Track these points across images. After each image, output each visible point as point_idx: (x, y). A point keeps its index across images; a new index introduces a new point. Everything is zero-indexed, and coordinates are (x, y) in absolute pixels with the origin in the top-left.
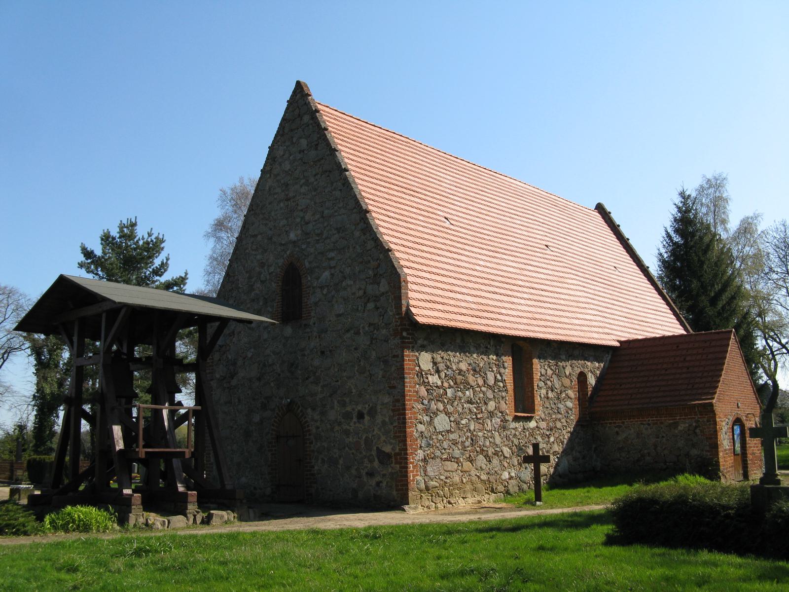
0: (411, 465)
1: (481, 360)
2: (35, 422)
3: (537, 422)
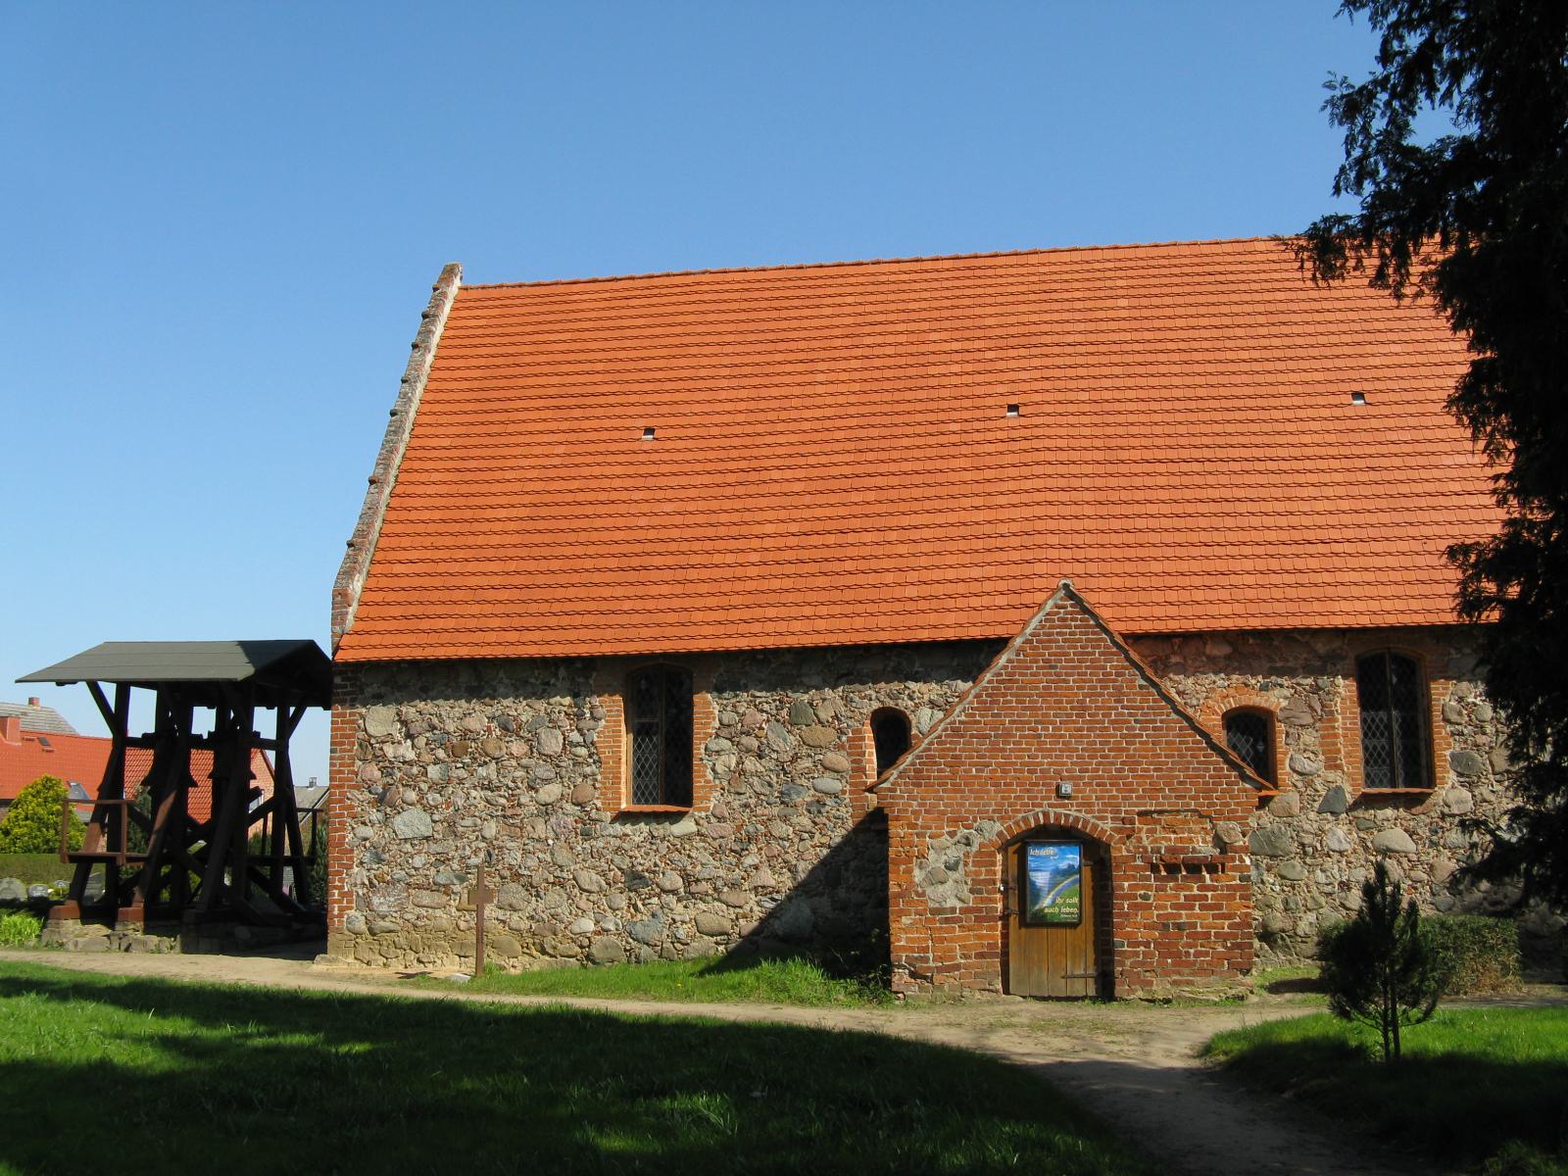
0: (336, 892)
1: (522, 710)
2: (1484, 100)
3: (697, 824)
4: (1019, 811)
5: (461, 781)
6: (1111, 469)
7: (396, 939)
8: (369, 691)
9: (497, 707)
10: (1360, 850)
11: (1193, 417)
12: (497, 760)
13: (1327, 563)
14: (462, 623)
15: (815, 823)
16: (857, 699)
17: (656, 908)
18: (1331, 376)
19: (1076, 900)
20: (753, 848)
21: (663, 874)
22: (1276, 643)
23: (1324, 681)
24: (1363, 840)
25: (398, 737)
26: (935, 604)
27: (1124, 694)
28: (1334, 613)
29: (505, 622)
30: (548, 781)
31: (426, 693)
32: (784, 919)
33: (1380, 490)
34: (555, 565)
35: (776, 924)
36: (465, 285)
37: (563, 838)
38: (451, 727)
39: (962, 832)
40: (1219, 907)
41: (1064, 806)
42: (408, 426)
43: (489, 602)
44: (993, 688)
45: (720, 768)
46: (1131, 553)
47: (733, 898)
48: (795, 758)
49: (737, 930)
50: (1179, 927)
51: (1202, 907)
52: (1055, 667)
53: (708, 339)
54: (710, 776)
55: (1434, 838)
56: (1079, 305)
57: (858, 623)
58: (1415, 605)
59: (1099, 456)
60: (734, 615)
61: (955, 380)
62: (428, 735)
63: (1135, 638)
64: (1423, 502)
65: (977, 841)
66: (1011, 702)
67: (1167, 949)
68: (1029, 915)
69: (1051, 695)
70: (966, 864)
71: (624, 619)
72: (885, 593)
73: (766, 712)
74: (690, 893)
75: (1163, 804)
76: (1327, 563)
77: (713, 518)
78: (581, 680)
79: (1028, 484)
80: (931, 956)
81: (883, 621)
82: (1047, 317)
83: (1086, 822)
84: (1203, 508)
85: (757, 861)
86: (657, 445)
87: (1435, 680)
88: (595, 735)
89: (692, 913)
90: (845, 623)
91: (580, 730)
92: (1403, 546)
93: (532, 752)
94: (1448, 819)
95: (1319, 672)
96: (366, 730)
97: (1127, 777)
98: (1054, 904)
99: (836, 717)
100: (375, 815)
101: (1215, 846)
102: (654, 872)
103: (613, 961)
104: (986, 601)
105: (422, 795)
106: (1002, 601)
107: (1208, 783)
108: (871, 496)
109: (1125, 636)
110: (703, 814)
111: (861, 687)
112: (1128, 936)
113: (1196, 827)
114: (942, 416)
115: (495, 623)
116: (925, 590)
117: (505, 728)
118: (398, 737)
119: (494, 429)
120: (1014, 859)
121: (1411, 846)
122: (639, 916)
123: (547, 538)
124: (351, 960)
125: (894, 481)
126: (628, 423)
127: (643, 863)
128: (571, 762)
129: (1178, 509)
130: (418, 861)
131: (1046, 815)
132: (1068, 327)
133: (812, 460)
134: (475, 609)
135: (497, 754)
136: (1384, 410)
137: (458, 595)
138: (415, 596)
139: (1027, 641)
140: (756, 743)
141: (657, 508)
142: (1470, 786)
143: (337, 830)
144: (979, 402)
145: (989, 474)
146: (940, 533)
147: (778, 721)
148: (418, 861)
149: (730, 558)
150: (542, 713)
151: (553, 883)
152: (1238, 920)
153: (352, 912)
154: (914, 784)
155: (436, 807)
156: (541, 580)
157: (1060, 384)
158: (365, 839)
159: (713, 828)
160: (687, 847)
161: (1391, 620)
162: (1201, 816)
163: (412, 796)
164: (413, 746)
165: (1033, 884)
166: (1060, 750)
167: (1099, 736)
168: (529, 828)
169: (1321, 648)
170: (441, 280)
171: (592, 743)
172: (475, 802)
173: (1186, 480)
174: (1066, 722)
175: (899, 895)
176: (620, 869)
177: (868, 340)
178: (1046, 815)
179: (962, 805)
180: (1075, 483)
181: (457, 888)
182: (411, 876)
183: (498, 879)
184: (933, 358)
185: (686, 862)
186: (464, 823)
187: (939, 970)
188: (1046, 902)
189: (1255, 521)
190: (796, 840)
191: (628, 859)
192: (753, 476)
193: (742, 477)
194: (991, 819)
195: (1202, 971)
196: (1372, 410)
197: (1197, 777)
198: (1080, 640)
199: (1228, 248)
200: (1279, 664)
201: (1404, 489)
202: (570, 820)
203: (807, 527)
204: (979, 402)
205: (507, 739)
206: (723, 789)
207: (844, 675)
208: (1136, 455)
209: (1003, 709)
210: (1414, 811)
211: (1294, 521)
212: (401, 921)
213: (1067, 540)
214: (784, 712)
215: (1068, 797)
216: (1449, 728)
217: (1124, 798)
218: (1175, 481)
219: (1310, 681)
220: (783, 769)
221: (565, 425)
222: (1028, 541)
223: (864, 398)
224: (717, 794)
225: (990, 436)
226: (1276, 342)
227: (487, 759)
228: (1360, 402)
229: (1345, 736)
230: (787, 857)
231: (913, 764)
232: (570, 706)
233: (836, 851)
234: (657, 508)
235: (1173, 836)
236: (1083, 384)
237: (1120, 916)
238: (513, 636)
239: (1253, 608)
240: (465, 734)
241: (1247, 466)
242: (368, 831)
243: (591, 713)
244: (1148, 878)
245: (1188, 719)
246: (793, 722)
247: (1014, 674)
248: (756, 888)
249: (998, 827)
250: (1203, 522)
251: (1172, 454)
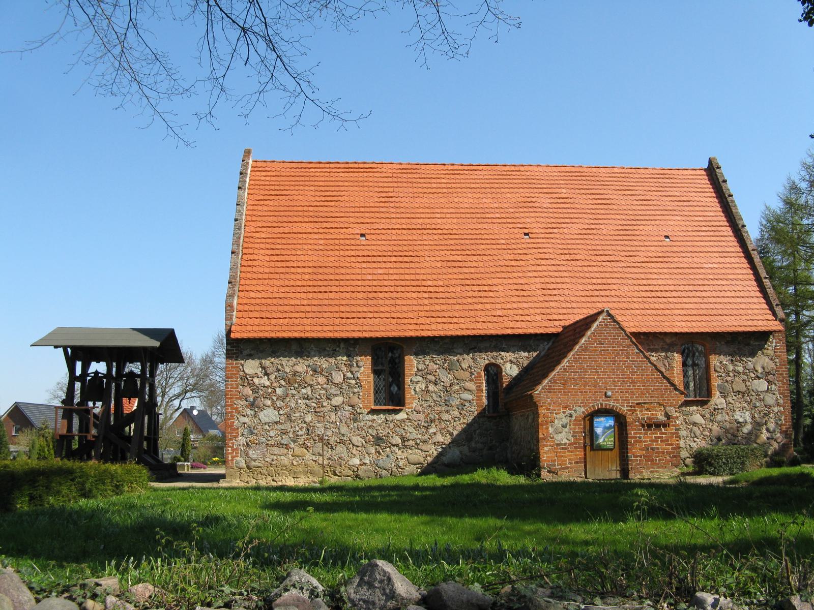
0: (230, 449)
1: (323, 363)
3: (407, 414)
4: (590, 403)
5: (293, 396)
6: (574, 263)
7: (262, 471)
8: (245, 352)
9: (310, 362)
10: (684, 423)
11: (603, 242)
12: (311, 386)
13: (667, 306)
14: (291, 321)
15: (461, 414)
16: (478, 359)
17: (389, 453)
18: (655, 228)
19: (613, 439)
20: (433, 425)
21: (392, 437)
22: (650, 338)
23: (669, 354)
24: (685, 419)
25: (260, 375)
26: (510, 318)
27: (630, 355)
28: (674, 327)
29: (313, 322)
30: (336, 395)
31: (275, 354)
32: (447, 456)
33: (682, 277)
34: (331, 295)
35: (444, 458)
36: (255, 159)
37: (344, 421)
38: (288, 370)
39: (568, 412)
40: (667, 441)
42: (243, 227)
43: (303, 312)
44: (579, 352)
45: (418, 389)
46: (588, 299)
47: (424, 447)
48: (451, 385)
49: (426, 462)
50: (653, 449)
51: (661, 441)
52: (603, 344)
53: (382, 194)
54: (413, 393)
55: (712, 418)
56: (545, 191)
57: (479, 326)
58: (704, 324)
59: (567, 257)
60: (422, 321)
61: (499, 221)
62: (276, 374)
63: (637, 335)
64: (700, 282)
65: (574, 415)
66: (586, 358)
67: (648, 458)
68: (595, 446)
69: (602, 355)
70: (570, 425)
71: (371, 321)
72: (488, 313)
73: (438, 364)
74: (405, 446)
75: (646, 400)
76: (667, 306)
77: (402, 277)
78: (351, 349)
79: (540, 268)
80: (556, 463)
81: (490, 325)
82: (533, 195)
83: (617, 407)
84: (614, 281)
85: (435, 431)
86: (529, 241)
87: (711, 355)
88: (359, 374)
89: (405, 455)
90: (473, 326)
91: (352, 372)
92: (695, 300)
93: (328, 382)
94: (717, 411)
95: (667, 351)
96: (244, 371)
97: (632, 389)
98: (604, 441)
99: (469, 367)
100: (249, 412)
101: (665, 417)
102: (388, 437)
103: (369, 478)
104: (532, 317)
105: (273, 403)
106: (539, 318)
107: (662, 391)
108: (472, 270)
109: (631, 333)
110: (410, 410)
111: (480, 354)
112: (633, 453)
114: (496, 236)
115: (308, 322)
116: (505, 312)
117: (315, 371)
118: (260, 375)
119: (286, 230)
120: (588, 423)
121: (703, 422)
122: (381, 456)
123: (325, 283)
124: (238, 481)
125: (481, 264)
126: (352, 231)
127: (383, 433)
128: (347, 387)
129: (604, 281)
130: (272, 433)
131: (602, 404)
132: (543, 200)
133: (442, 253)
134: (297, 315)
135: (311, 383)
136: (678, 244)
137: (286, 308)
138: (264, 308)
139: (593, 333)
140: (434, 378)
141: (375, 271)
142: (725, 397)
143: (230, 419)
144: (511, 231)
145: (522, 263)
146: (506, 287)
147: (443, 368)
148: (272, 433)
149: (414, 295)
150: (333, 364)
151: (340, 443)
152: (674, 446)
153: (238, 459)
154: (548, 392)
155: (281, 408)
156: (326, 302)
157: (544, 225)
158: (244, 423)
159: (415, 416)
160: (403, 425)
161: (696, 330)
162: (660, 405)
163: (269, 403)
164: (268, 379)
165: (596, 433)
166: (606, 378)
167: (621, 372)
168: (327, 417)
169: (668, 341)
170: (244, 156)
171: (358, 378)
172: (301, 405)
173: (605, 269)
174: (609, 367)
175: (543, 438)
176: (372, 435)
177: (456, 200)
178: (602, 404)
179: (568, 401)
180: (560, 268)
181: (292, 446)
182: (268, 441)
183: (312, 441)
184: (487, 210)
185: (403, 432)
186: (295, 415)
187: (560, 469)
188: (601, 440)
189: (636, 288)
190: (452, 421)
191: (375, 431)
192: (417, 259)
193: (412, 259)
194: (580, 406)
195: (661, 467)
196: (674, 244)
197: (658, 389)
198: (613, 333)
199: (603, 170)
200: (652, 347)
201: (692, 277)
202: (347, 413)
203: (447, 283)
204: (511, 231)
205: (316, 376)
206: (419, 399)
207: (473, 348)
208: (583, 257)
209: (583, 361)
210: (704, 407)
211: (651, 288)
212: (263, 462)
213: (561, 292)
214: (446, 365)
215: (610, 397)
216: (717, 374)
217: (631, 397)
218: (601, 269)
219: (664, 354)
220: (446, 390)
221: (321, 231)
222: (545, 292)
223: (459, 226)
224: (416, 401)
225: (519, 246)
226: (630, 212)
227: (306, 385)
228: (668, 240)
229: (677, 377)
230: (449, 429)
231: (548, 383)
232: (346, 361)
233: (469, 425)
234: (375, 271)
235: (649, 413)
236: (554, 225)
237: (630, 445)
238: (319, 328)
239: (642, 324)
240: (295, 373)
241: (629, 264)
242: (246, 420)
243: (357, 364)
244: (641, 430)
245: (655, 366)
246: (450, 369)
247: (587, 347)
248: (434, 443)
249: (583, 409)
250: (615, 287)
251: (597, 258)
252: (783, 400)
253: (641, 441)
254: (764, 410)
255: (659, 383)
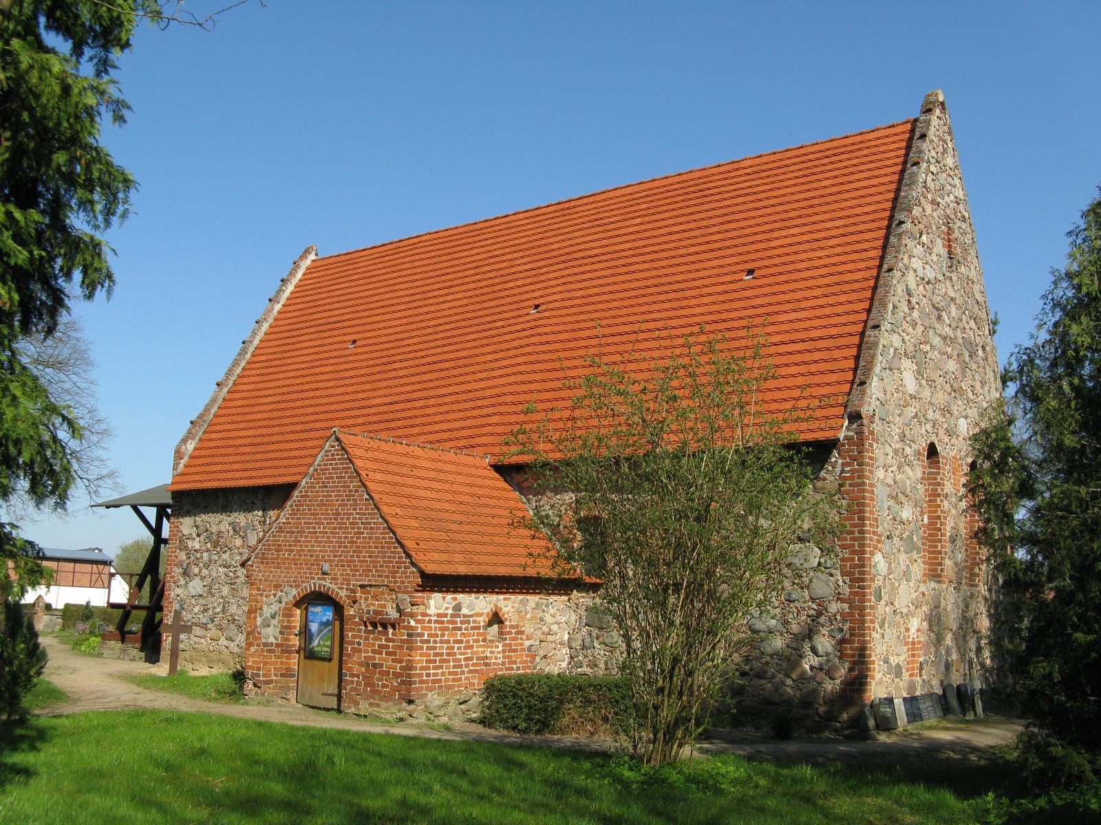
1: (241, 518)
8: (185, 508)
19: (329, 643)
40: (394, 654)
41: (324, 579)
50: (375, 665)
83: (333, 591)
98: (319, 645)
100: (182, 582)
107: (393, 567)
113: (388, 598)
163: (196, 570)
188: (316, 643)
197: (390, 562)
217: (353, 575)
249: (294, 592)
252: (850, 587)
253: (360, 651)
254: (810, 608)
255: (391, 552)
